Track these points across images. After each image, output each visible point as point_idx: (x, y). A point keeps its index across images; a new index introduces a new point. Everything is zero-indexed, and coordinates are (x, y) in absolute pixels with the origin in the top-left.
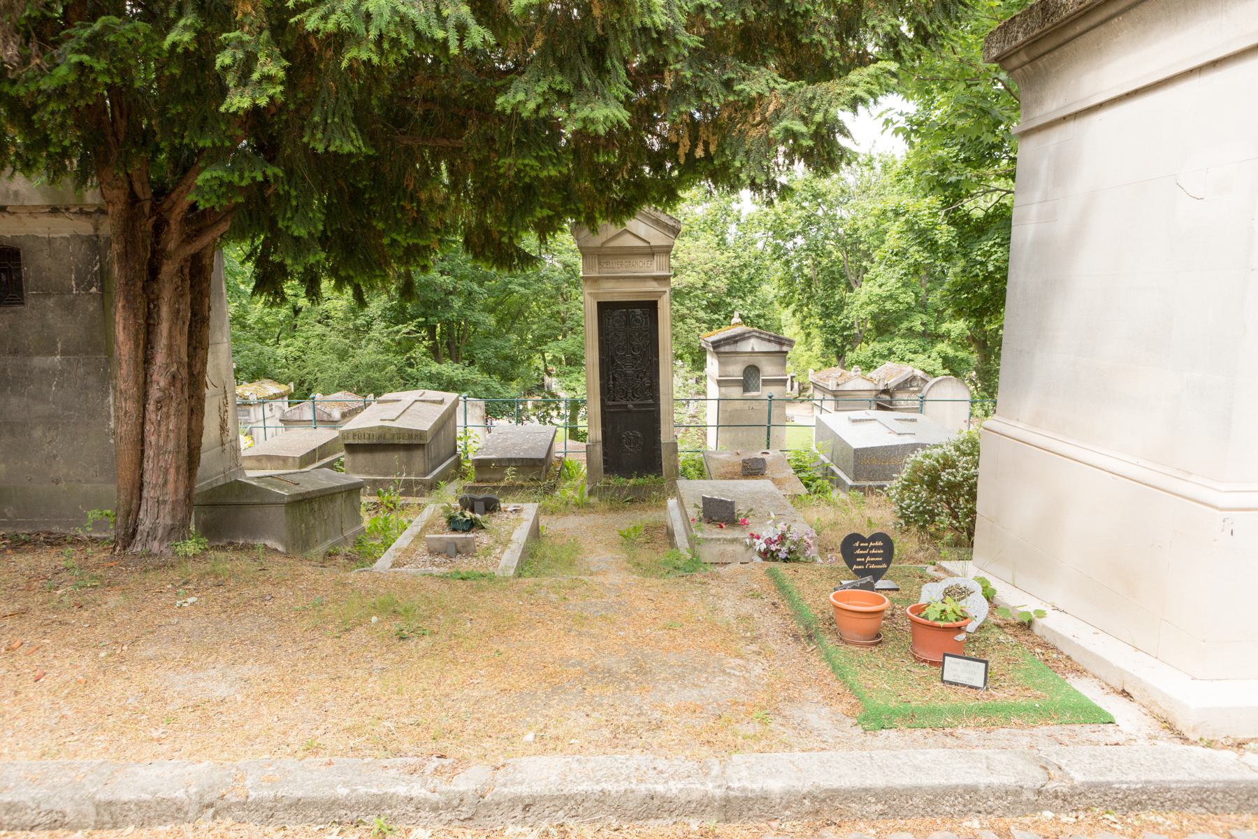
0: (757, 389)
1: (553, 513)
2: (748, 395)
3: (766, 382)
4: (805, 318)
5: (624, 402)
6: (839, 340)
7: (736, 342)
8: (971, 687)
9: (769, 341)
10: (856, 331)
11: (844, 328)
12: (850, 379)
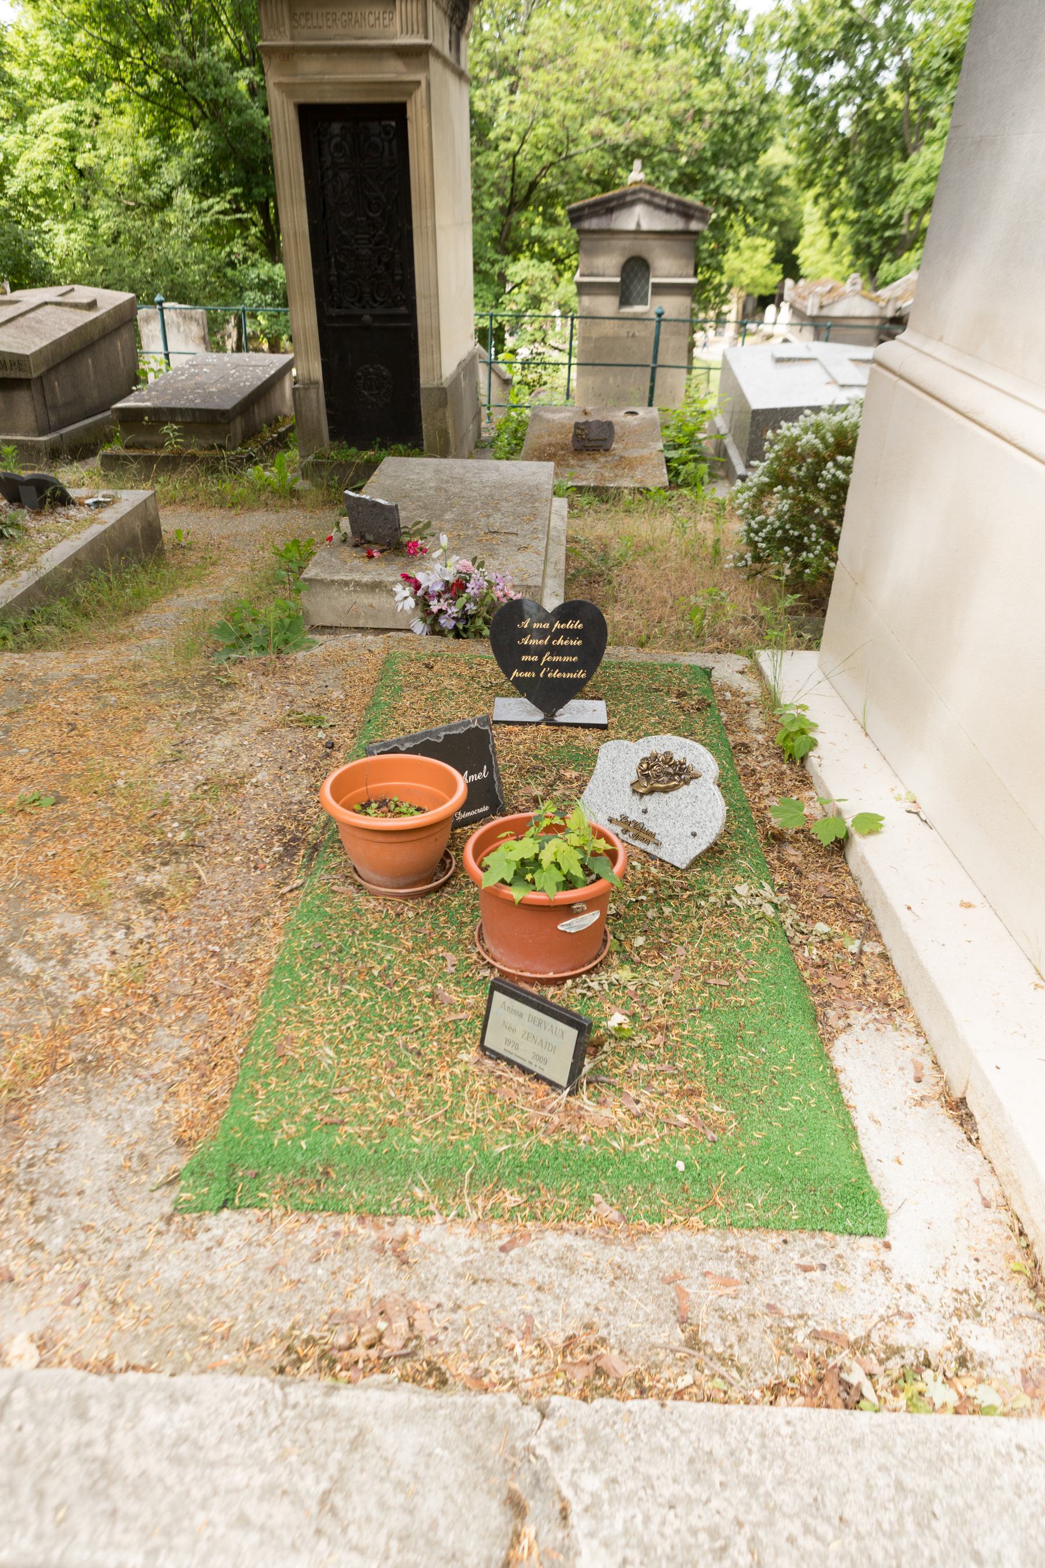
0: (644, 302)
1: (233, 505)
2: (628, 310)
3: (660, 289)
4: (833, 208)
5: (356, 310)
6: (876, 246)
7: (610, 211)
8: (538, 1078)
9: (668, 210)
10: (904, 231)
11: (886, 226)
12: (842, 296)
